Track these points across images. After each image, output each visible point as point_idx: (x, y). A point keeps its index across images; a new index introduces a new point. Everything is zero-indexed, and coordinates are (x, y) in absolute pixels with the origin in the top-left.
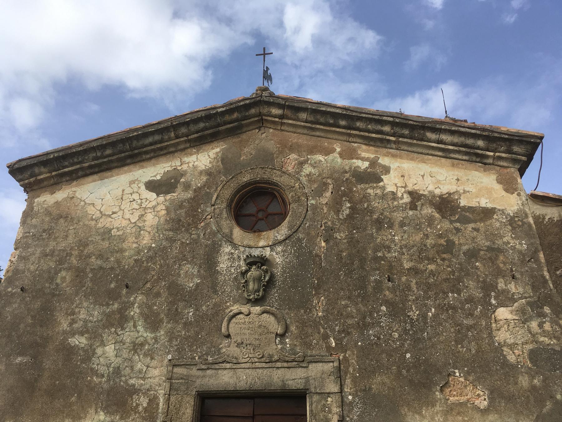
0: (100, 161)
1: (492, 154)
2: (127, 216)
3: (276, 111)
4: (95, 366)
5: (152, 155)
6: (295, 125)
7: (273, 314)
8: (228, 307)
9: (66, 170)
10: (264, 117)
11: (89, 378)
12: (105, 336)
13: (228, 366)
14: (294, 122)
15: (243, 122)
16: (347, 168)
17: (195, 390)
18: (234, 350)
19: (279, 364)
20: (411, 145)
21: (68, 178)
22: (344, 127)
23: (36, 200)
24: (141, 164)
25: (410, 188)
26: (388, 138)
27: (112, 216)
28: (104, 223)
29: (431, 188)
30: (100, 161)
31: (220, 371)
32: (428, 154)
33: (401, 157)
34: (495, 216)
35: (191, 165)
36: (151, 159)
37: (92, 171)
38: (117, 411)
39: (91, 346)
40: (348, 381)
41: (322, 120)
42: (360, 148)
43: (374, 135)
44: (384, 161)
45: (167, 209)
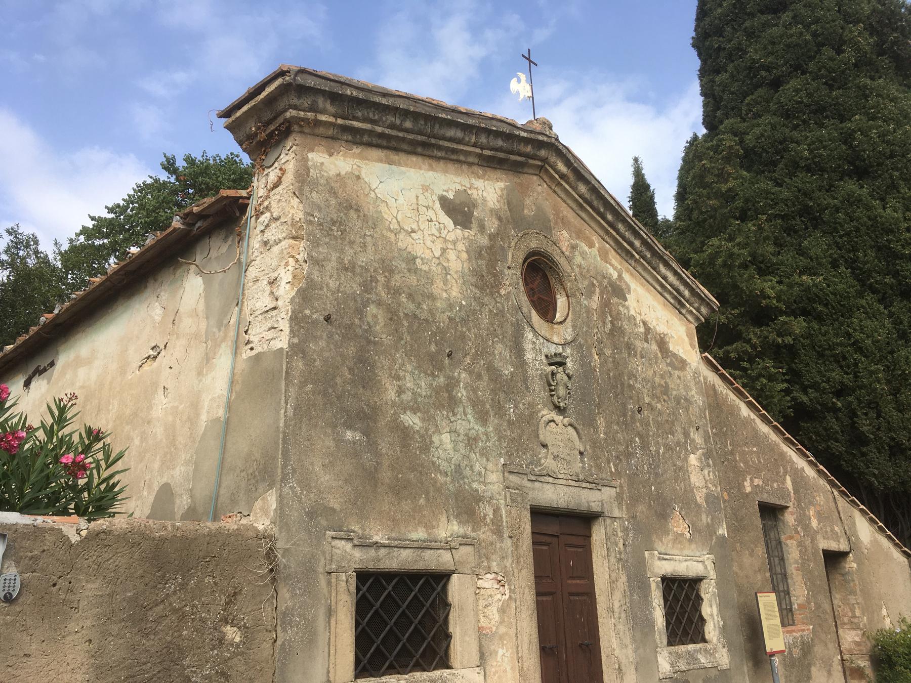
1: (688, 306)
3: (561, 167)
4: (435, 459)
6: (570, 193)
8: (539, 411)
9: (356, 124)
10: (546, 166)
11: (433, 475)
12: (438, 418)
13: (551, 480)
14: (570, 190)
15: (531, 161)
17: (529, 504)
18: (549, 463)
20: (645, 269)
21: (350, 138)
25: (643, 317)
26: (634, 253)
27: (413, 235)
29: (654, 323)
30: (394, 133)
31: (545, 485)
32: (651, 285)
36: (439, 159)
37: (379, 141)
38: (469, 522)
39: (427, 430)
43: (625, 244)
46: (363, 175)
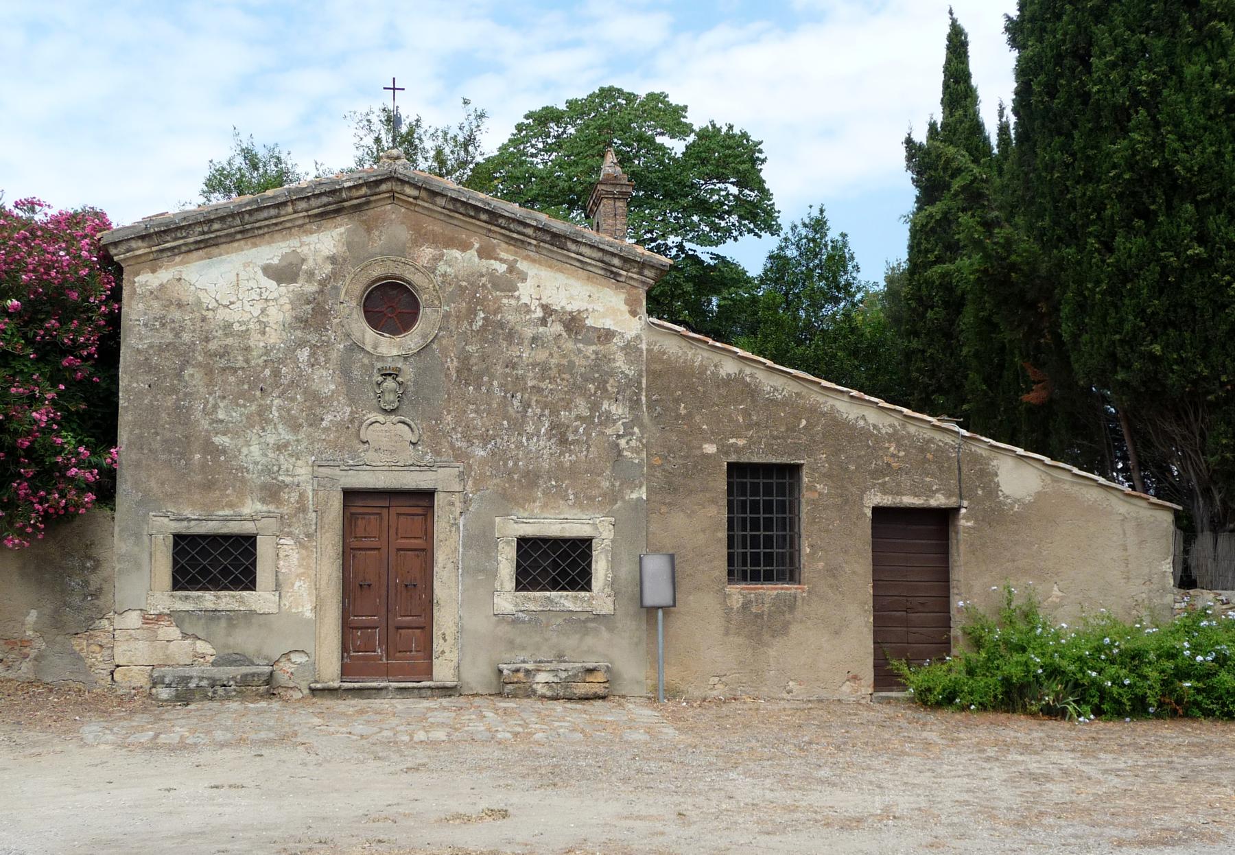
0: (207, 236)
1: (624, 273)
2: (248, 308)
3: (408, 190)
5: (266, 230)
7: (409, 425)
15: (372, 198)
16: (484, 270)
19: (412, 468)
20: (551, 251)
22: (485, 222)
23: (136, 280)
24: (254, 240)
25: (544, 302)
26: (529, 240)
28: (222, 314)
30: (207, 236)
33: (540, 263)
34: (614, 340)
35: (312, 247)
40: (470, 482)
41: (462, 210)
42: (499, 246)
43: (515, 235)
44: (522, 265)
45: (291, 303)
46: (184, 276)
